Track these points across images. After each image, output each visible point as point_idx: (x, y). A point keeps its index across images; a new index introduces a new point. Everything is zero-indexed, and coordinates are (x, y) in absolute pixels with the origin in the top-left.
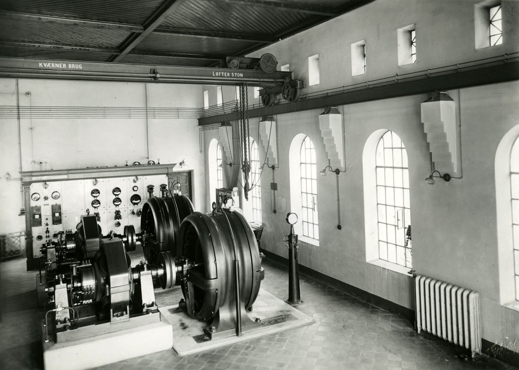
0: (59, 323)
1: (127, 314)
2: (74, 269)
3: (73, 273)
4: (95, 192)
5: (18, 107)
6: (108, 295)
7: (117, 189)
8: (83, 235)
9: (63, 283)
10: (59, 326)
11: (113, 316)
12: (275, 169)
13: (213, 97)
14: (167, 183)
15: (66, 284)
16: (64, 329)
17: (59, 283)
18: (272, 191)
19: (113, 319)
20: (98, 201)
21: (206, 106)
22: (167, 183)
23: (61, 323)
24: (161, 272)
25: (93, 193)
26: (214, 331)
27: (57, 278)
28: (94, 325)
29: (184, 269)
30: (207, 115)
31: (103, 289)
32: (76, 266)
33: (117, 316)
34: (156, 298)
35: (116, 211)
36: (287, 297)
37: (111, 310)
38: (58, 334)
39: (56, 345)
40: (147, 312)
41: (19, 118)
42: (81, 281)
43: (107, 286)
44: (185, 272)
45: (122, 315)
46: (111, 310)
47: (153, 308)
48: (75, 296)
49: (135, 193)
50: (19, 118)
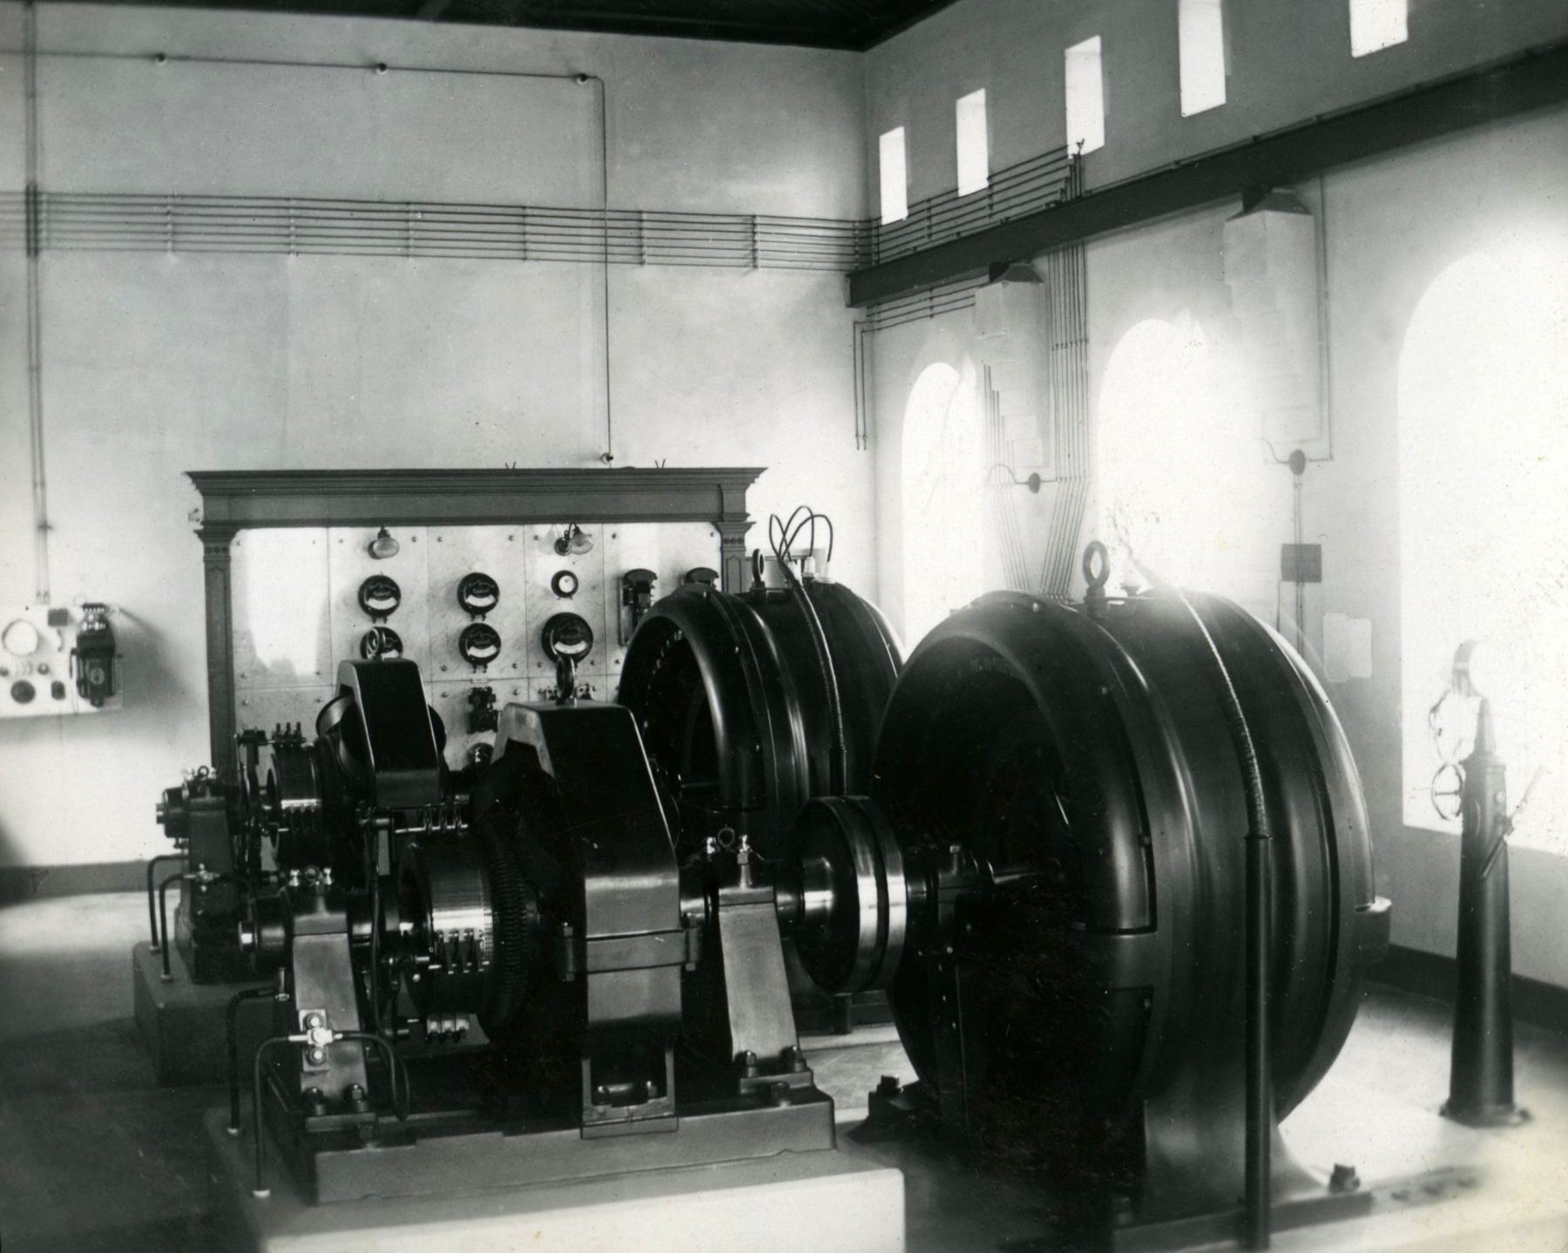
0: (319, 1109)
1: (662, 1092)
2: (383, 835)
3: (374, 863)
4: (380, 586)
5: (33, 197)
6: (570, 978)
7: (479, 584)
8: (357, 749)
9: (332, 906)
10: (319, 1121)
11: (597, 1098)
12: (1309, 466)
13: (933, 148)
14: (714, 563)
15: (341, 917)
16: (349, 1138)
17: (310, 908)
18: (1290, 587)
19: (594, 1112)
20: (390, 634)
21: (894, 208)
22: (714, 563)
23: (328, 1112)
24: (818, 899)
25: (370, 595)
26: (1123, 1218)
27: (295, 883)
28: (498, 1135)
29: (941, 895)
30: (889, 251)
31: (544, 949)
32: (389, 828)
33: (618, 1101)
34: (798, 1036)
35: (476, 691)
36: (1443, 1094)
37: (586, 1067)
38: (323, 1156)
39: (313, 1212)
40: (765, 1096)
41: (33, 250)
42: (419, 911)
43: (568, 930)
44: (943, 911)
45: (638, 1096)
46: (586, 1067)
47: (794, 1080)
48: (391, 981)
49: (565, 606)
50: (33, 250)
